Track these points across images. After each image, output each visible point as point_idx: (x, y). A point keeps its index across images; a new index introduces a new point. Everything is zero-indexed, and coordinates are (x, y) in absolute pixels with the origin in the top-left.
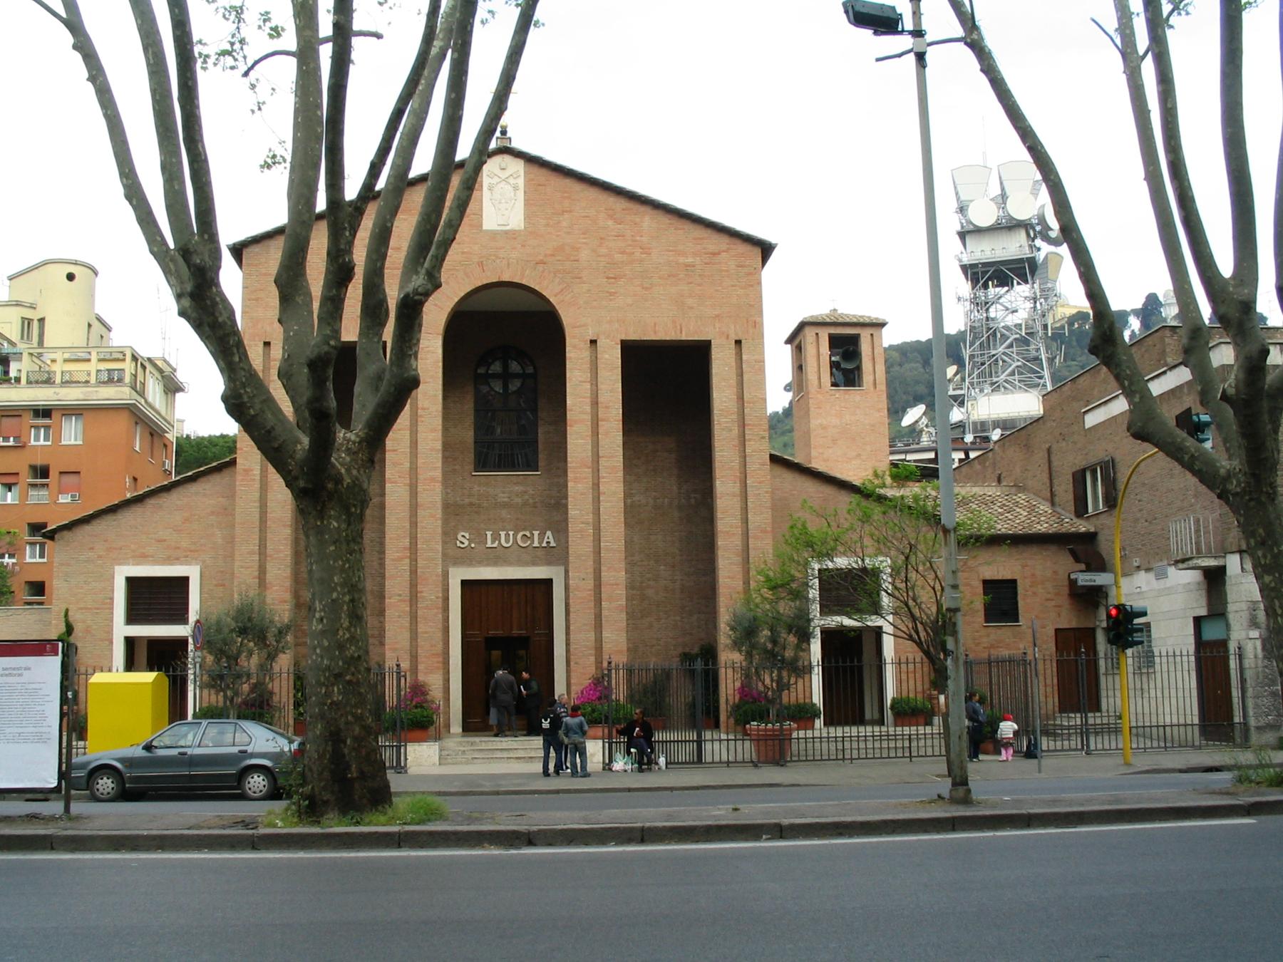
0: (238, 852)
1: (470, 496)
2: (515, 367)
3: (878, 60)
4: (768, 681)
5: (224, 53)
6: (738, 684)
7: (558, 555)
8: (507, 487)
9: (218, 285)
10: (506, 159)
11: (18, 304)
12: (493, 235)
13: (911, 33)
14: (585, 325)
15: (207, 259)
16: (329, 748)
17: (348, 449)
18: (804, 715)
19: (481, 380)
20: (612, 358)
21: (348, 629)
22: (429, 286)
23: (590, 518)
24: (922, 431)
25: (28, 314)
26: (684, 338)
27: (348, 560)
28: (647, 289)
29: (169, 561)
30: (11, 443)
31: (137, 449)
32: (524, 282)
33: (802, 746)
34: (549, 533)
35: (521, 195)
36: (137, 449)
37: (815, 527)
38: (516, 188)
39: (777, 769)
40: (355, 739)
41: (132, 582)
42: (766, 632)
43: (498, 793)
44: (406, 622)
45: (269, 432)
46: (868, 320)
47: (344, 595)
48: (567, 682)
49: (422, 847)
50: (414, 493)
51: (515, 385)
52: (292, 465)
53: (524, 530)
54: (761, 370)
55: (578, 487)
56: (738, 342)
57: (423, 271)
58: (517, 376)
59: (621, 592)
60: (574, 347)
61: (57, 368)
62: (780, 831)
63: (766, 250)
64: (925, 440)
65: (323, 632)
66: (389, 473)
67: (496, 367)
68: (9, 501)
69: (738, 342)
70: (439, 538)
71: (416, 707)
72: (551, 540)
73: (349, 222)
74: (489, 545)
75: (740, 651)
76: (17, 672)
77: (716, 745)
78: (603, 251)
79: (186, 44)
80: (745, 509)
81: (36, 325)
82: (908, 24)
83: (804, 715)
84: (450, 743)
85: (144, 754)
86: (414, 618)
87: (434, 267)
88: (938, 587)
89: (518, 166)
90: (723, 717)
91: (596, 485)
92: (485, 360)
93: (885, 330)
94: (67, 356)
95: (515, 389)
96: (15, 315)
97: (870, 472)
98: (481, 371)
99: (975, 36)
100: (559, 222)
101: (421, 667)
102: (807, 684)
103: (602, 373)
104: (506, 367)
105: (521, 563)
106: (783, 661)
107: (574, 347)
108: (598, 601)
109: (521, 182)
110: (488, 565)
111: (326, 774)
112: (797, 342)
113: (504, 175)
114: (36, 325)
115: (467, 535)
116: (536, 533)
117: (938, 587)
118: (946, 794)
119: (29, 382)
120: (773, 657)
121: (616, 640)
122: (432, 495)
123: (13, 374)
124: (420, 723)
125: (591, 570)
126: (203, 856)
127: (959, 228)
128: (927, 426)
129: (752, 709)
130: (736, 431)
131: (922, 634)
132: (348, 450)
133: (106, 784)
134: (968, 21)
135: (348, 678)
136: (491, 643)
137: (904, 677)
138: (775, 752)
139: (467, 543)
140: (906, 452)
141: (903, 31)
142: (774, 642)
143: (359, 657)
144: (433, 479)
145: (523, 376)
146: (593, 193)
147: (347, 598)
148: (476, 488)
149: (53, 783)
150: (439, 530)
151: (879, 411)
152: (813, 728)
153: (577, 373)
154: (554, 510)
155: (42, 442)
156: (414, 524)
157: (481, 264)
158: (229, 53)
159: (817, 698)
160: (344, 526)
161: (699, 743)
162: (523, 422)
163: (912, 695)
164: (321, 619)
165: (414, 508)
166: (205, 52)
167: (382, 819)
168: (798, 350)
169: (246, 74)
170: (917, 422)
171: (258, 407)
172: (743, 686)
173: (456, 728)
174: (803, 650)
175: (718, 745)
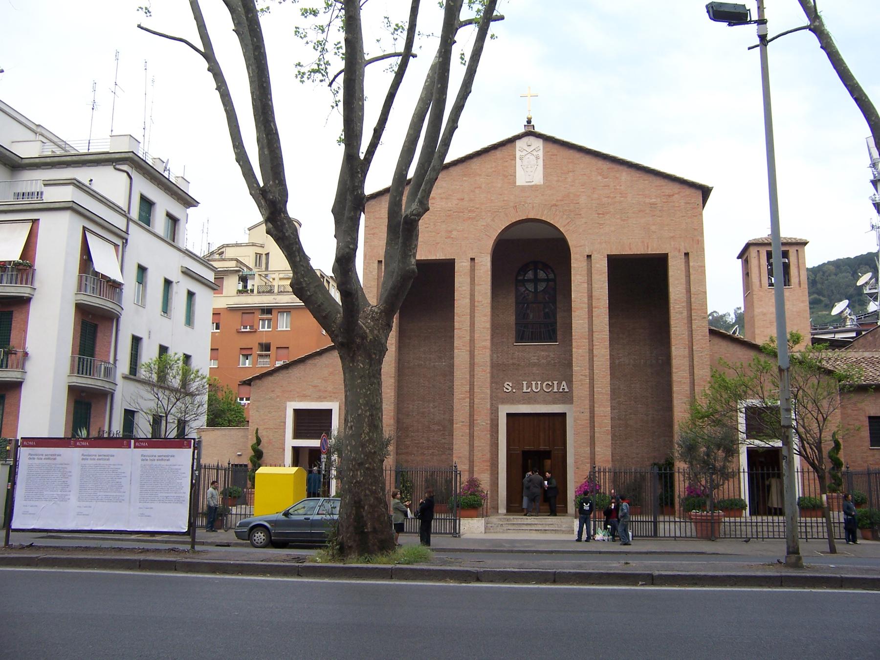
0: (288, 577)
2: (542, 275)
3: (749, 49)
4: (703, 482)
5: (315, 71)
6: (687, 485)
7: (567, 397)
8: (536, 352)
9: (286, 212)
10: (531, 139)
11: (254, 245)
12: (523, 188)
13: (755, 22)
14: (584, 245)
15: (277, 196)
16: (354, 512)
17: (372, 317)
18: (734, 507)
19: (519, 283)
20: (601, 266)
21: (368, 434)
22: (421, 210)
23: (587, 372)
24: (846, 317)
25: (259, 250)
27: (369, 389)
28: (624, 220)
29: (320, 399)
30: (248, 330)
34: (564, 383)
37: (731, 377)
38: (537, 158)
39: (710, 542)
40: (371, 506)
41: (297, 412)
42: (704, 449)
43: (512, 551)
44: (466, 439)
45: (319, 306)
46: (794, 241)
47: (366, 411)
48: (574, 481)
49: (406, 579)
50: (472, 356)
51: (541, 287)
52: (334, 327)
54: (703, 273)
55: (579, 350)
56: (687, 254)
57: (417, 200)
59: (608, 421)
60: (576, 260)
61: (276, 283)
62: (652, 580)
63: (705, 192)
64: (849, 324)
65: (352, 436)
66: (457, 343)
67: (530, 275)
68: (247, 365)
69: (687, 254)
70: (488, 385)
71: (471, 494)
72: (565, 387)
73: (361, 168)
74: (525, 390)
75: (685, 462)
76: (167, 458)
77: (667, 524)
78: (595, 196)
79: (261, 61)
80: (692, 367)
81: (264, 257)
82: (755, 16)
83: (734, 507)
84: (494, 519)
85: (284, 518)
86: (472, 436)
87: (423, 197)
88: (820, 418)
89: (539, 143)
90: (677, 507)
91: (591, 351)
92: (524, 269)
93: (806, 247)
94: (282, 276)
96: (252, 251)
97: (768, 339)
98: (520, 278)
99: (817, 24)
100: (566, 178)
102: (737, 485)
103: (595, 277)
104: (536, 274)
105: (546, 402)
106: (714, 468)
107: (576, 260)
108: (592, 427)
110: (524, 403)
111: (351, 529)
112: (744, 258)
113: (530, 149)
114: (264, 257)
116: (555, 383)
117: (820, 418)
118: (783, 561)
119: (259, 292)
120: (708, 466)
121: (604, 455)
122: (484, 356)
123: (249, 287)
124: (473, 504)
125: (588, 407)
126: (310, 580)
127: (872, 178)
128: (850, 315)
129: (697, 500)
130: (685, 314)
131: (809, 450)
132: (373, 318)
133: (260, 537)
134: (812, 12)
136: (526, 454)
137: (806, 482)
138: (709, 531)
139: (510, 389)
140: (835, 333)
141: (751, 21)
142: (708, 455)
143: (375, 452)
144: (485, 347)
146: (588, 159)
149: (185, 529)
150: (489, 380)
151: (803, 302)
152: (740, 516)
153: (578, 277)
154: (564, 368)
155: (266, 329)
156: (472, 376)
158: (318, 71)
159: (745, 495)
160: (367, 367)
161: (655, 523)
162: (547, 310)
163: (813, 496)
164: (351, 427)
165: (472, 365)
166: (302, 71)
167: (385, 559)
168: (746, 263)
169: (330, 85)
170: (842, 312)
171: (312, 289)
172: (689, 487)
173: (502, 510)
174: (729, 462)
175: (669, 526)
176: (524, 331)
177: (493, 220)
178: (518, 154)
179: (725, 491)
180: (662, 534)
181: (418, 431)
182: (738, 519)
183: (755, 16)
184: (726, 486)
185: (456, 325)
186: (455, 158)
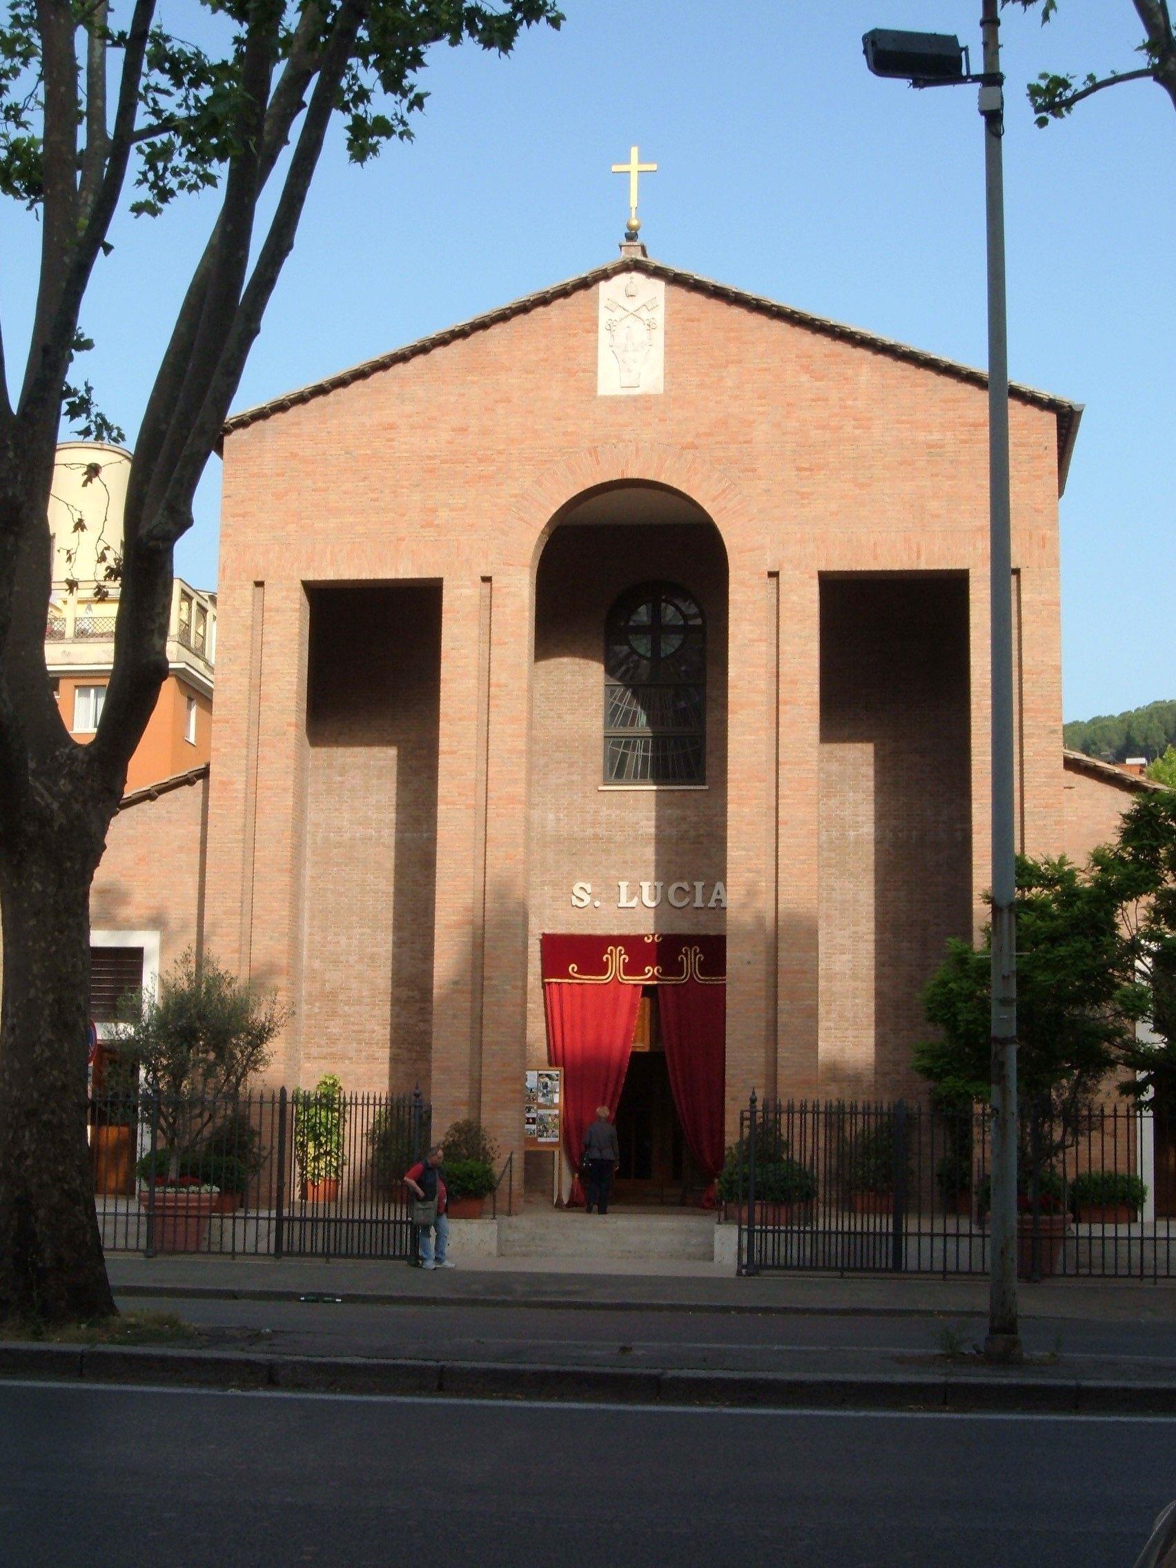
1: (594, 824)
10: (637, 278)
12: (615, 404)
13: (976, 79)
20: (805, 603)
26: (923, 566)
28: (861, 486)
31: (192, 739)
32: (663, 479)
33: (1136, 1250)
35: (659, 337)
36: (192, 739)
38: (650, 327)
51: (670, 645)
53: (681, 879)
58: (674, 629)
67: (643, 614)
77: (926, 1241)
82: (977, 66)
95: (671, 650)
100: (721, 379)
101: (485, 1098)
104: (656, 614)
109: (659, 316)
115: (588, 887)
116: (699, 885)
135: (45, 1117)
139: (587, 899)
143: (64, 1088)
144: (984, 686)
145: (686, 630)
147: (50, 998)
148: (605, 812)
157: (593, 451)
160: (51, 890)
176: (624, 755)
177: (538, 483)
178: (604, 316)
179: (1086, 1157)
180: (912, 1264)
181: (359, 1002)
182: (1123, 1231)
183: (977, 66)
184: (1083, 1147)
185: (444, 743)
186: (263, 402)
